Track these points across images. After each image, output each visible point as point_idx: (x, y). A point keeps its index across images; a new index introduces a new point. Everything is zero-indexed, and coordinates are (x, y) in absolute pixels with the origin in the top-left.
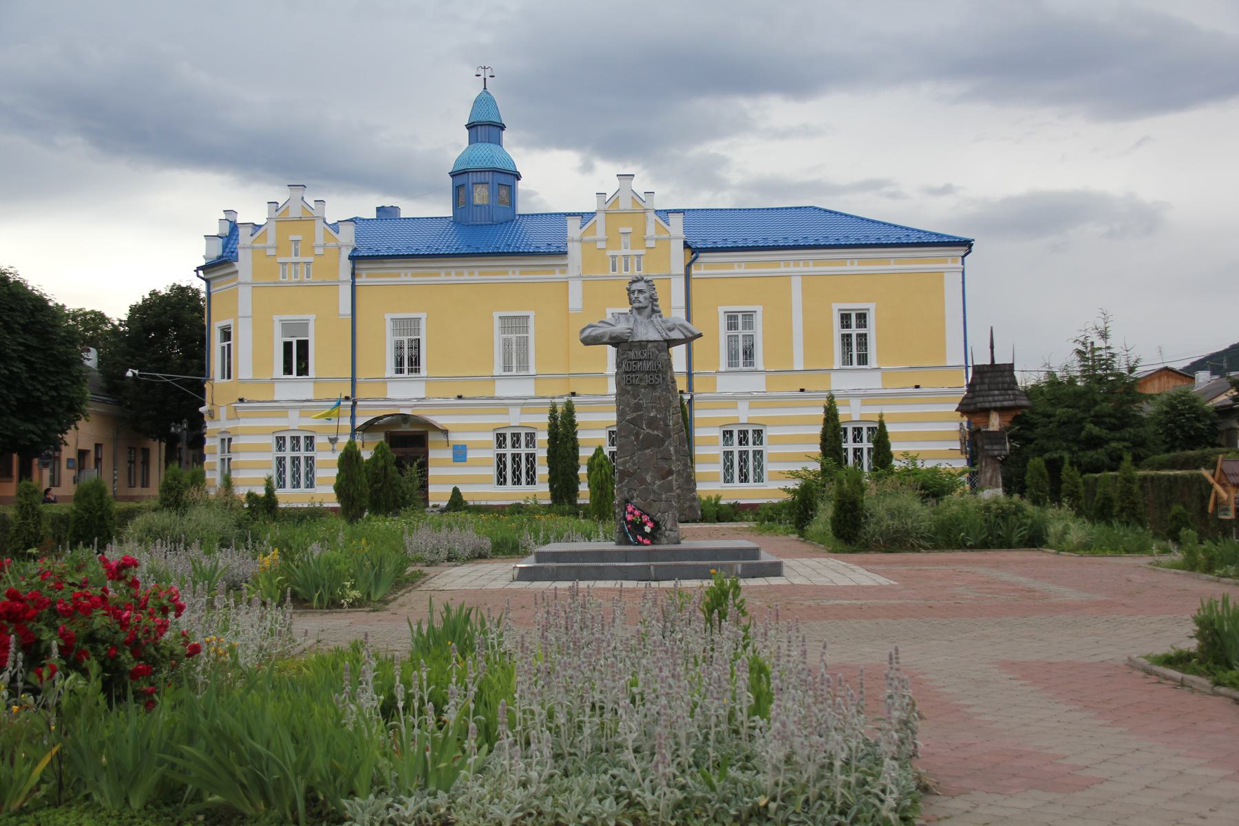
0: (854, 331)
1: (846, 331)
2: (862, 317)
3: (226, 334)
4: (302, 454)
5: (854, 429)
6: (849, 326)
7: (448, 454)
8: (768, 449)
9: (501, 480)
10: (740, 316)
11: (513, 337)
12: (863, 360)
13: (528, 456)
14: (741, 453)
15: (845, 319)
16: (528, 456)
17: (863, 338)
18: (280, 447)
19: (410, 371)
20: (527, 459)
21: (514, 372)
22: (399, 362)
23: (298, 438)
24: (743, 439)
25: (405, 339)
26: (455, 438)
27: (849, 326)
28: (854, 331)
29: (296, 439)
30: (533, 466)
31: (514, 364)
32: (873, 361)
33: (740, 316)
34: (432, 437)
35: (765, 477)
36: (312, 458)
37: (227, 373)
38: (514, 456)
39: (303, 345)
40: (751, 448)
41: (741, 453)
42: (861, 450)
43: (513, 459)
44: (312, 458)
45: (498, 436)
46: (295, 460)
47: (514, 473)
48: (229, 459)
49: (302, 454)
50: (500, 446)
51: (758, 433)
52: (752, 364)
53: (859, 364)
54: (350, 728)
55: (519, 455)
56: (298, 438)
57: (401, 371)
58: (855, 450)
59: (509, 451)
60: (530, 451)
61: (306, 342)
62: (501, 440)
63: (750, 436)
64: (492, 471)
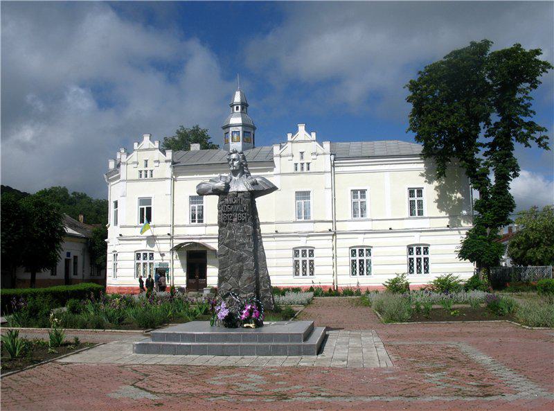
0: (416, 199)
1: (419, 199)
3: (116, 203)
4: (422, 256)
8: (373, 259)
9: (296, 273)
10: (416, 190)
11: (196, 206)
12: (420, 213)
13: (425, 259)
14: (360, 261)
15: (411, 192)
16: (425, 259)
18: (410, 252)
19: (199, 222)
20: (417, 261)
21: (303, 219)
22: (193, 217)
23: (420, 249)
24: (418, 252)
25: (145, 207)
30: (427, 264)
31: (303, 215)
32: (425, 214)
33: (359, 192)
36: (428, 258)
37: (116, 223)
38: (303, 261)
39: (149, 210)
40: (365, 258)
41: (360, 261)
42: (420, 259)
44: (428, 258)
45: (409, 249)
46: (304, 262)
49: (422, 256)
50: (353, 256)
51: (369, 251)
53: (419, 215)
54: (120, 387)
56: (146, 254)
57: (194, 221)
58: (417, 259)
60: (426, 256)
61: (151, 208)
62: (353, 253)
63: (365, 252)
64: (292, 270)
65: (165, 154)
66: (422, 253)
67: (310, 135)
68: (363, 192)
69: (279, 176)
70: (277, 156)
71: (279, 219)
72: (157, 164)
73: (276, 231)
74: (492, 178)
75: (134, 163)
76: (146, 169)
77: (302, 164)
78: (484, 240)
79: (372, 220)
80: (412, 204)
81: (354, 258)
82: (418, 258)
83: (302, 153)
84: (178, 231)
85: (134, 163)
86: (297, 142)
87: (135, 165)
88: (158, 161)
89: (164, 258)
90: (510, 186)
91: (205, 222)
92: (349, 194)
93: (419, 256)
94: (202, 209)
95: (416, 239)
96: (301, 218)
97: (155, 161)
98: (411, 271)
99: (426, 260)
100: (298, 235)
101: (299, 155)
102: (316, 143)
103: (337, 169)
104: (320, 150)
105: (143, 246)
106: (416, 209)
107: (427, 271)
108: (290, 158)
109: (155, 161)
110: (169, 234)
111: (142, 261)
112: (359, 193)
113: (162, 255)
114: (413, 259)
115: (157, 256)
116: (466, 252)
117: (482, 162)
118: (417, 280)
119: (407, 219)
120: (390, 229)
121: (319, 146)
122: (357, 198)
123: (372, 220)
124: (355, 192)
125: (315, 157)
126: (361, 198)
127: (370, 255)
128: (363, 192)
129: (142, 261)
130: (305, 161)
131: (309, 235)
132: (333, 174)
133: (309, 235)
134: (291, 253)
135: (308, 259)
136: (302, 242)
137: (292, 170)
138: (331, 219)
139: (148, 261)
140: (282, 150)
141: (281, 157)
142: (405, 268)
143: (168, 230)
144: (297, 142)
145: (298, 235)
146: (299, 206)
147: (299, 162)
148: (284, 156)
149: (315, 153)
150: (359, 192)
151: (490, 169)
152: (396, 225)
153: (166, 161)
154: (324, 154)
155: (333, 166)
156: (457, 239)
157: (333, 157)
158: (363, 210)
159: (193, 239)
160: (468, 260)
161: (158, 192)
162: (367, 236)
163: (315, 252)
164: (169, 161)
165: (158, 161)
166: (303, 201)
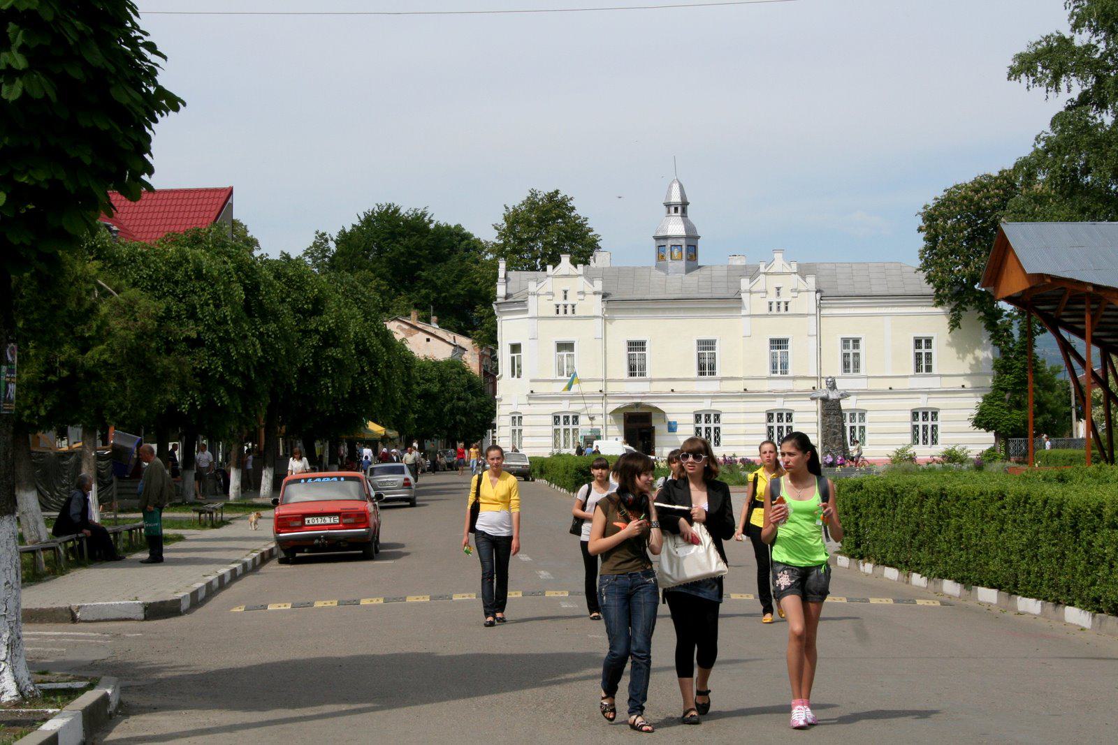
0: (923, 351)
2: (929, 341)
4: (712, 425)
5: (565, 417)
6: (920, 348)
7: (665, 427)
12: (929, 369)
13: (715, 429)
14: (779, 428)
15: (918, 342)
16: (715, 429)
17: (929, 356)
19: (854, 371)
20: (715, 431)
22: (774, 367)
23: (568, 417)
26: (671, 418)
27: (920, 348)
28: (923, 351)
29: (708, 416)
30: (718, 435)
32: (935, 370)
33: (851, 342)
34: (654, 415)
35: (721, 443)
36: (719, 428)
38: (707, 429)
42: (782, 427)
43: (706, 431)
44: (719, 428)
45: (555, 417)
46: (925, 427)
47: (927, 433)
48: (520, 431)
49: (712, 425)
50: (556, 424)
52: (858, 371)
55: (709, 428)
57: (704, 374)
59: (775, 424)
60: (717, 425)
61: (931, 353)
63: (571, 419)
65: (592, 284)
66: (571, 423)
67: (576, 267)
68: (856, 341)
69: (749, 318)
70: (745, 292)
71: (747, 375)
72: (582, 297)
73: (745, 390)
74: (1015, 330)
75: (548, 293)
76: (565, 302)
77: (779, 303)
78: (1002, 407)
79: (868, 377)
80: (918, 357)
81: (557, 427)
82: (924, 424)
83: (778, 289)
84: (612, 388)
85: (548, 293)
86: (772, 274)
87: (551, 297)
88: (583, 293)
89: (594, 422)
90: (1037, 343)
91: (648, 376)
92: (839, 343)
93: (780, 424)
94: (713, 357)
95: (922, 402)
96: (563, 375)
97: (579, 293)
98: (915, 441)
99: (934, 428)
100: (773, 395)
101: (775, 291)
102: (797, 276)
103: (824, 312)
104: (589, 288)
105: (564, 407)
106: (923, 363)
107: (935, 442)
108: (764, 295)
109: (579, 293)
110: (601, 391)
111: (562, 427)
112: (636, 346)
113: (592, 419)
114: (918, 426)
115: (583, 420)
116: (982, 422)
117: (1006, 313)
118: (924, 453)
119: (912, 376)
120: (890, 388)
121: (800, 279)
122: (849, 348)
123: (868, 377)
124: (845, 341)
125: (795, 294)
126: (854, 348)
127: (937, 420)
128: (856, 341)
129: (562, 427)
130: (783, 299)
131: (787, 395)
132: (819, 316)
133: (787, 395)
134: (764, 417)
135: (929, 423)
136: (705, 405)
137: (766, 311)
138: (815, 375)
139: (571, 427)
140: (753, 283)
141: (538, 295)
142: (908, 438)
143: (600, 386)
144: (772, 274)
145: (773, 395)
146: (774, 356)
147: (775, 300)
148: (755, 292)
149: (796, 290)
150: (851, 342)
151: (1014, 322)
152: (898, 384)
153: (595, 293)
154: (808, 291)
155: (819, 307)
156: (971, 404)
157: (818, 295)
158: (785, 366)
159: (633, 397)
160: (983, 430)
161: (582, 333)
162: (861, 397)
163: (794, 416)
164: (599, 293)
165: (583, 293)
166: (779, 351)
